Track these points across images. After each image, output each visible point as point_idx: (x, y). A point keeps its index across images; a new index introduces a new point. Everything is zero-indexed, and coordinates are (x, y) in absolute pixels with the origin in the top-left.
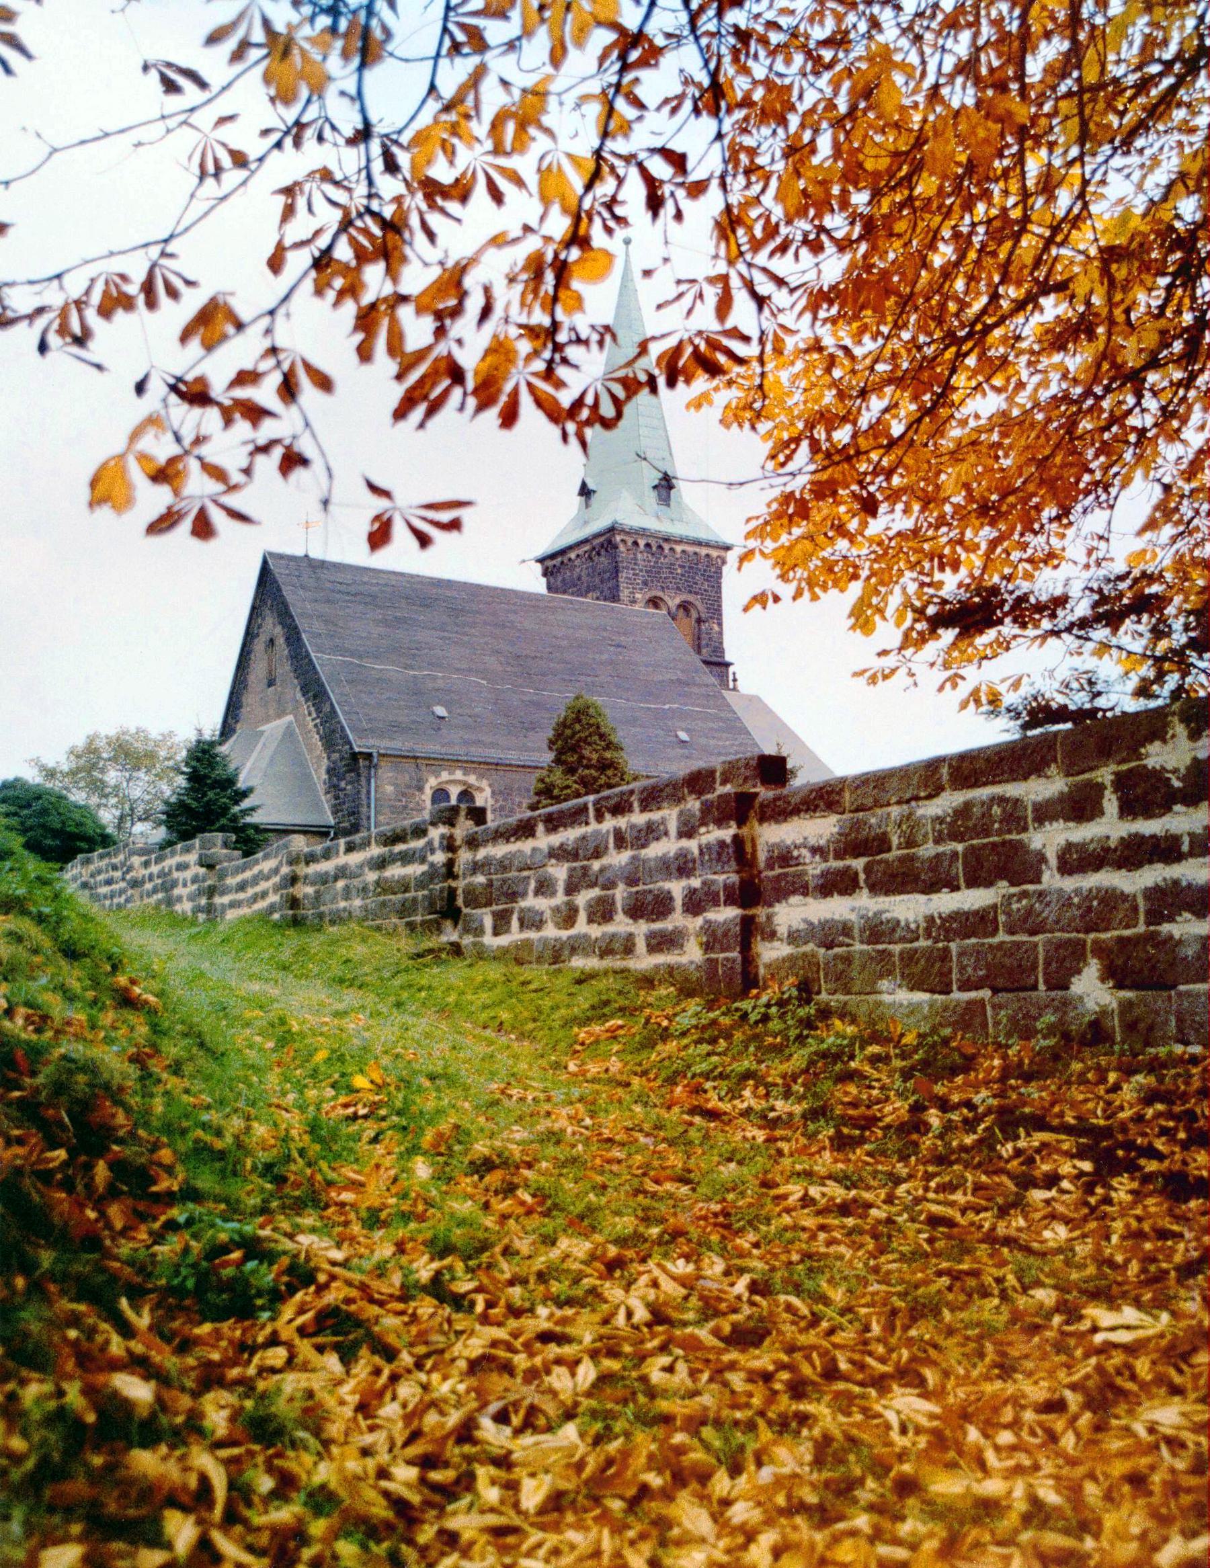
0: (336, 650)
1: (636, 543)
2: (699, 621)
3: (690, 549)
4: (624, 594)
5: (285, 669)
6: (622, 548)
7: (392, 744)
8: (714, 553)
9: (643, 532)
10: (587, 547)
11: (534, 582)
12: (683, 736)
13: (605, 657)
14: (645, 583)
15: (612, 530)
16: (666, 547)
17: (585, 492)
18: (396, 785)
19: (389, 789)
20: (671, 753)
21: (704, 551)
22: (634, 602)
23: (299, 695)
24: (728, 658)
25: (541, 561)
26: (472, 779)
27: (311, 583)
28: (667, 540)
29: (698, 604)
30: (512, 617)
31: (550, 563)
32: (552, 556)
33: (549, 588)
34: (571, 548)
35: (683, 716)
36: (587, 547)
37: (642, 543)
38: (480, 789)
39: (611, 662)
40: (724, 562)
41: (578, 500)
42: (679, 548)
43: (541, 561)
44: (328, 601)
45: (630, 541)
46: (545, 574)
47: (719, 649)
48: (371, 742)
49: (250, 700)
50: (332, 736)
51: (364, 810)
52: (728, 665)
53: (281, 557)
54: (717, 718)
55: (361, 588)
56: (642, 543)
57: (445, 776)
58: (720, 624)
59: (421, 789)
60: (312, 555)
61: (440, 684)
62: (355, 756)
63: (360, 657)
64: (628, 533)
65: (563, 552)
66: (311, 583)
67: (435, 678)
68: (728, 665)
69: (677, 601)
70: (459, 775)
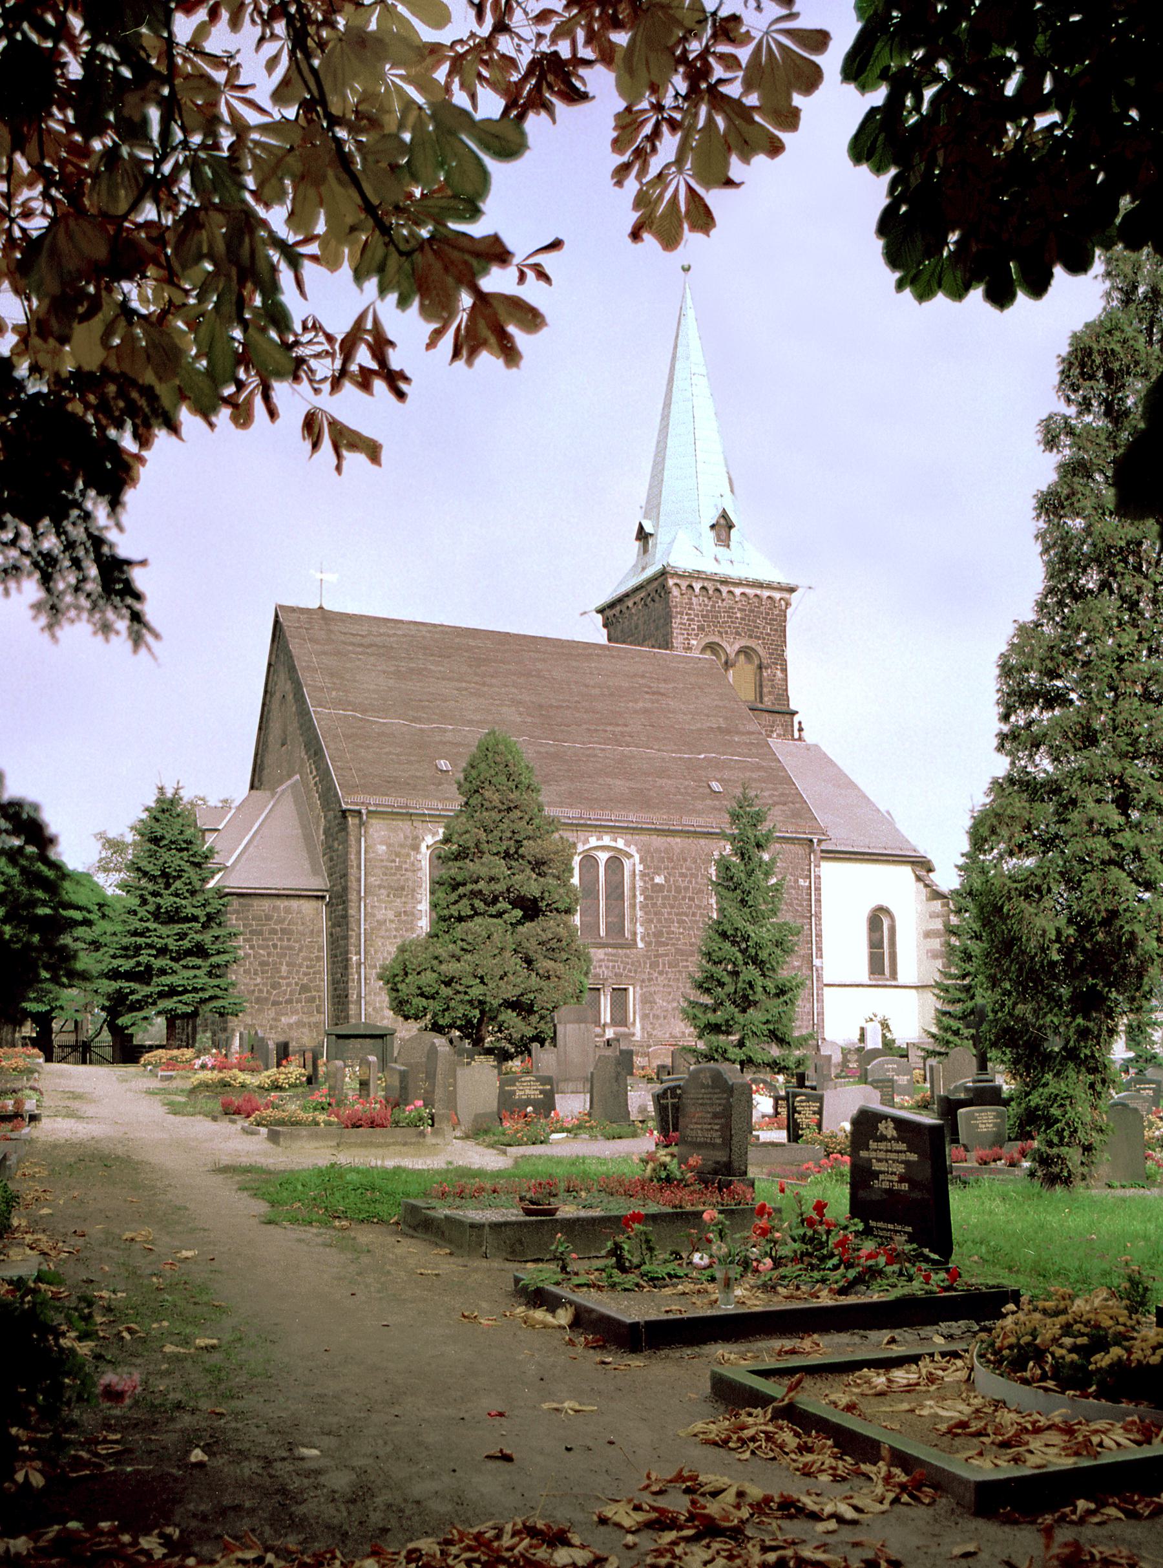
0: (339, 703)
1: (690, 587)
2: (760, 667)
3: (750, 592)
4: (678, 641)
5: (293, 727)
6: (675, 592)
7: (390, 800)
8: (777, 595)
9: (697, 575)
10: (643, 594)
11: (600, 636)
12: (716, 786)
13: (640, 705)
14: (701, 628)
15: (663, 574)
16: (724, 589)
17: (643, 536)
18: (389, 845)
19: (382, 848)
20: (699, 805)
21: (766, 593)
22: (689, 648)
23: (303, 754)
24: (793, 706)
25: (601, 611)
26: (620, 844)
27: (322, 635)
28: (725, 582)
29: (760, 649)
30: (539, 666)
31: (610, 613)
32: (612, 605)
33: (609, 640)
34: (627, 595)
35: (719, 765)
36: (643, 594)
37: (697, 586)
38: (630, 856)
39: (646, 711)
40: (788, 604)
41: (637, 545)
42: (738, 591)
43: (601, 611)
44: (338, 653)
45: (684, 584)
46: (605, 626)
47: (784, 696)
48: (361, 798)
49: (270, 759)
50: (328, 795)
51: (353, 871)
52: (794, 713)
53: (293, 610)
54: (760, 768)
55: (378, 640)
56: (697, 586)
57: (593, 842)
58: (784, 671)
59: (416, 848)
60: (326, 607)
61: (449, 737)
62: (344, 812)
63: (364, 712)
64: (680, 576)
65: (620, 600)
66: (322, 635)
67: (445, 731)
68: (794, 713)
69: (737, 647)
70: (607, 840)
